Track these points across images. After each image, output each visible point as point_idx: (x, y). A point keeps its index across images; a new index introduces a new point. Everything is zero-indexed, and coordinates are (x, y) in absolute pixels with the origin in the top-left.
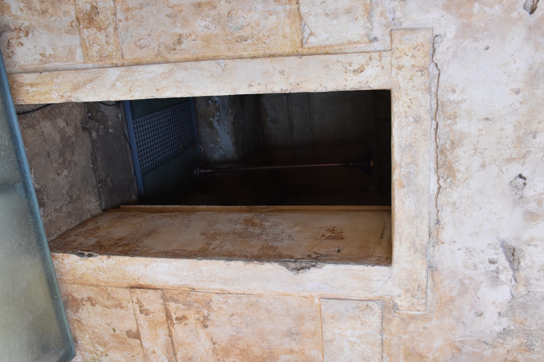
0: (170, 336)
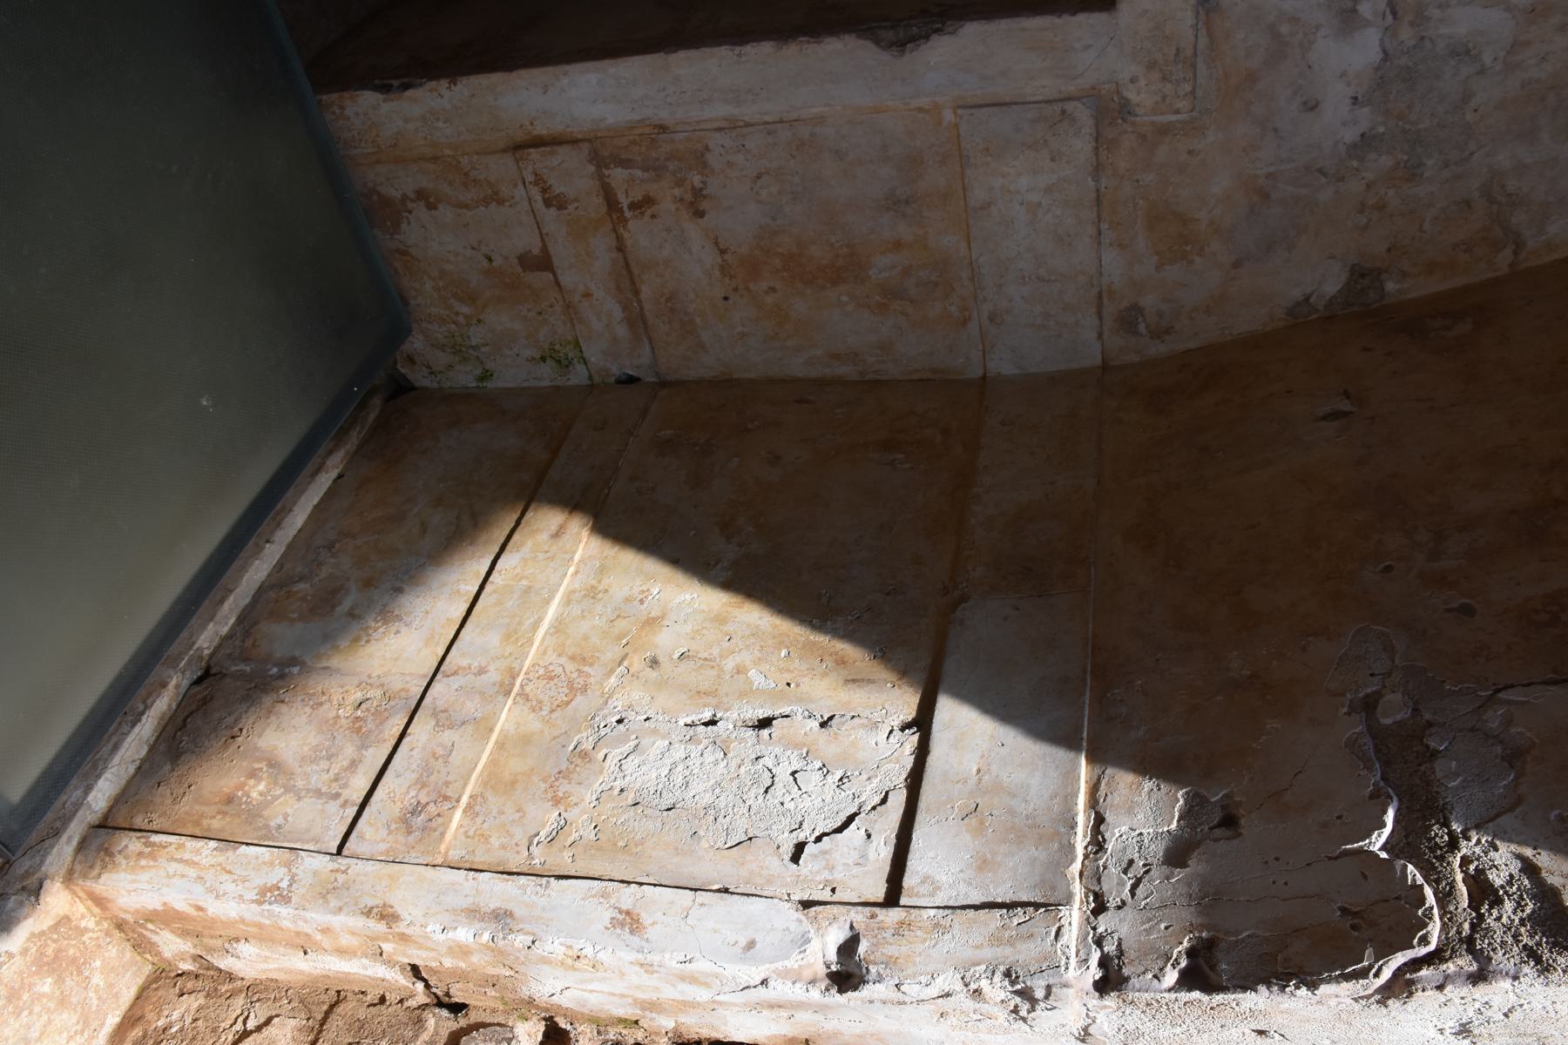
0: (621, 249)
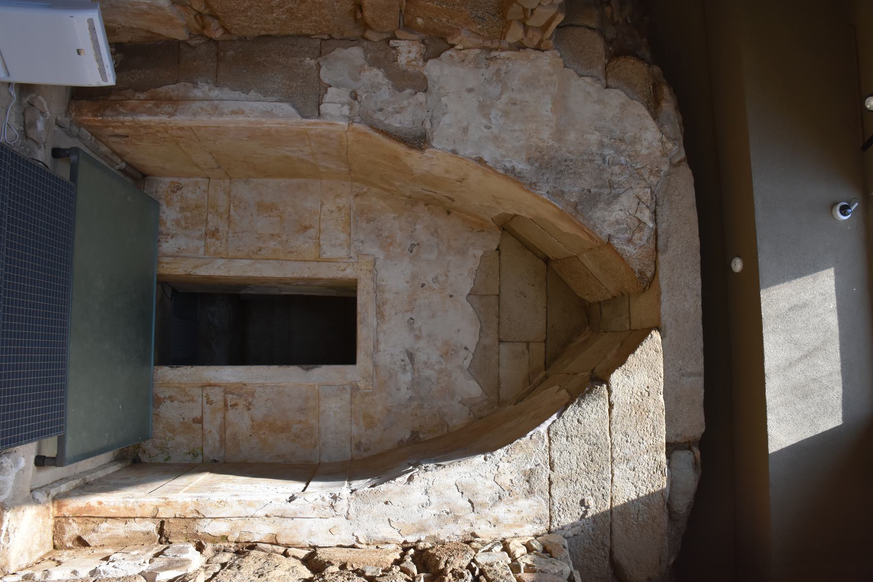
0: (224, 418)
